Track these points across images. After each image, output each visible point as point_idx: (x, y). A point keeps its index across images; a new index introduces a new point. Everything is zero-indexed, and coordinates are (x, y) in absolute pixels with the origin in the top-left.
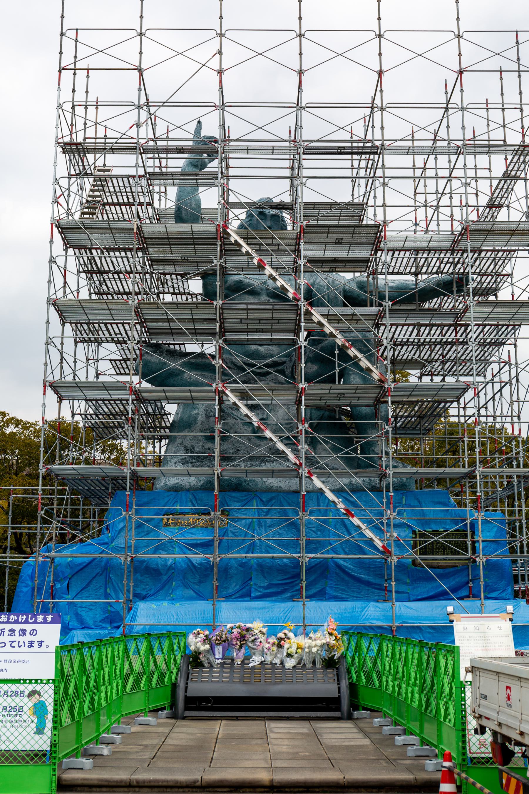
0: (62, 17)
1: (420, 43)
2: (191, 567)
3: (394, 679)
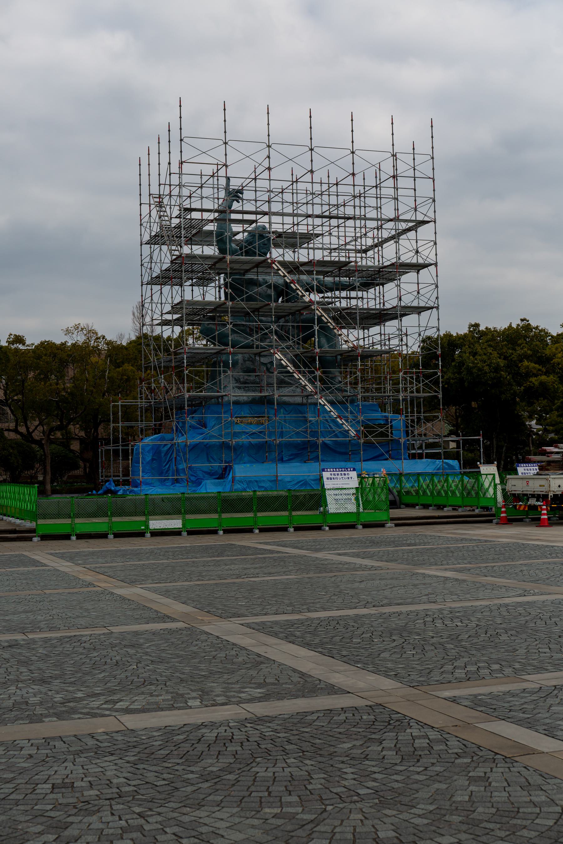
0: (159, 164)
1: (291, 152)
2: (251, 445)
3: (30, 503)
